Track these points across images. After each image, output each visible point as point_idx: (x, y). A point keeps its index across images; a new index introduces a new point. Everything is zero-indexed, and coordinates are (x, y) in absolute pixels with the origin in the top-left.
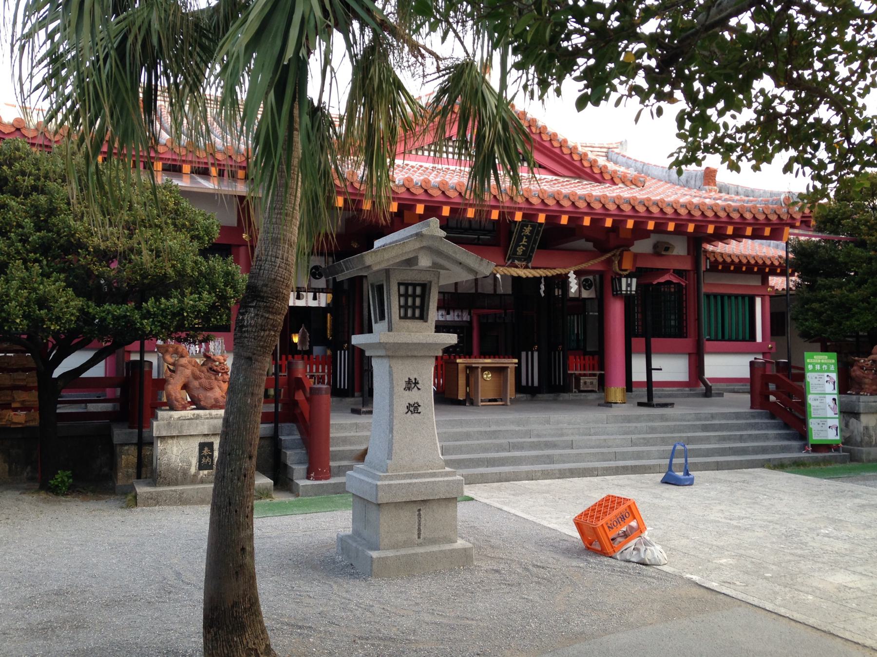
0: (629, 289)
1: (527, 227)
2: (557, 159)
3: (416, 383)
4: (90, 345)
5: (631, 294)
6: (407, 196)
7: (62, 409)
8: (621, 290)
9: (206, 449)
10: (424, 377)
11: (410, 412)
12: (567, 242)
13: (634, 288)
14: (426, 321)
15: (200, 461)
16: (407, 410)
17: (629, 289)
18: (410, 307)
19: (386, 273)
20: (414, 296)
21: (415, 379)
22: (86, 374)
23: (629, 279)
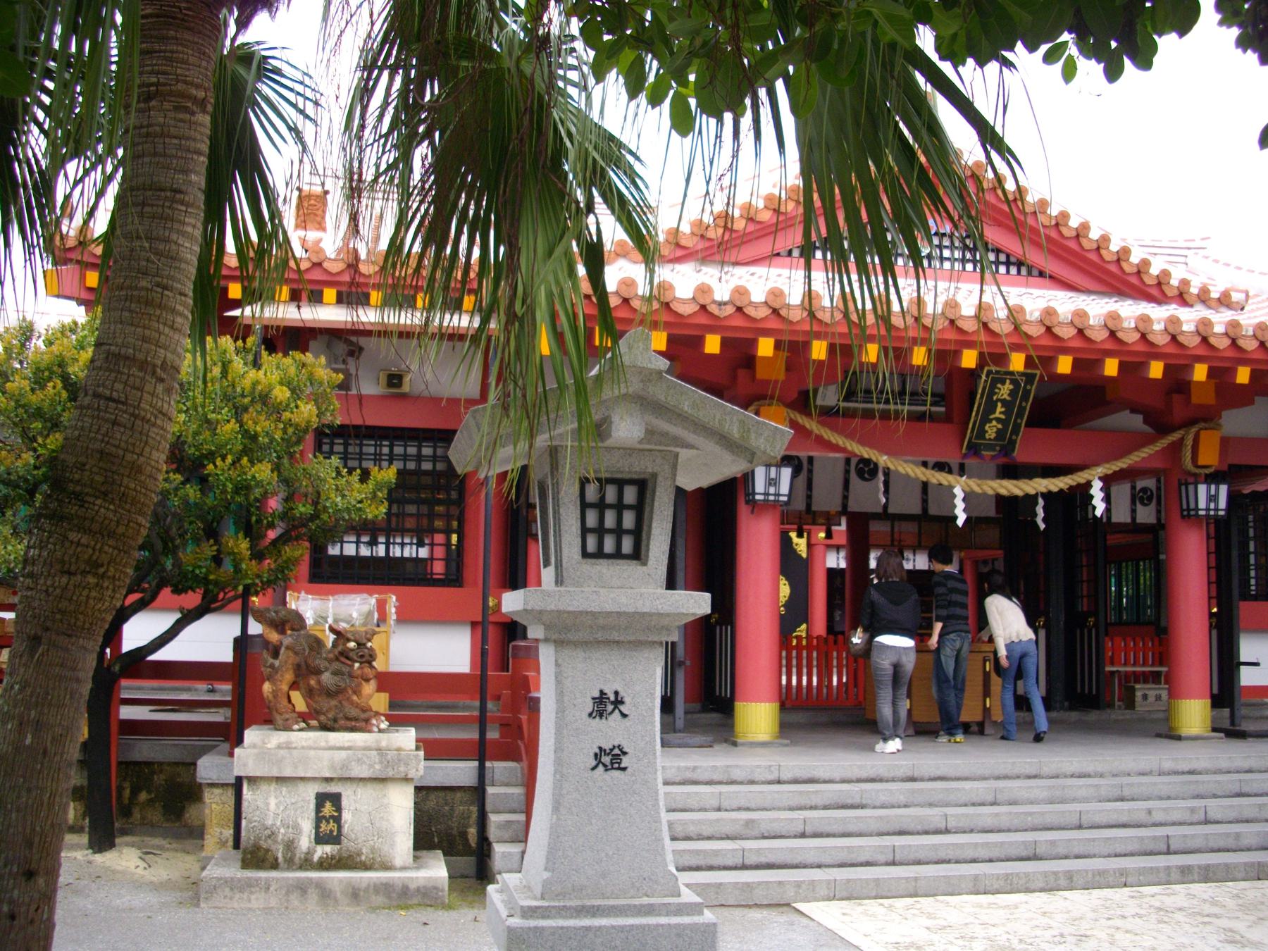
0: (1212, 506)
1: (1003, 383)
2: (1064, 255)
3: (618, 702)
4: (153, 605)
5: (1216, 515)
6: (739, 322)
7: (127, 713)
8: (1197, 509)
9: (328, 805)
10: (637, 688)
11: (601, 768)
12: (1092, 419)
13: (1222, 503)
14: (645, 564)
15: (317, 827)
16: (594, 763)
17: (1212, 506)
18: (610, 531)
19: (551, 455)
20: (620, 507)
21: (616, 693)
22: (160, 655)
23: (1213, 487)
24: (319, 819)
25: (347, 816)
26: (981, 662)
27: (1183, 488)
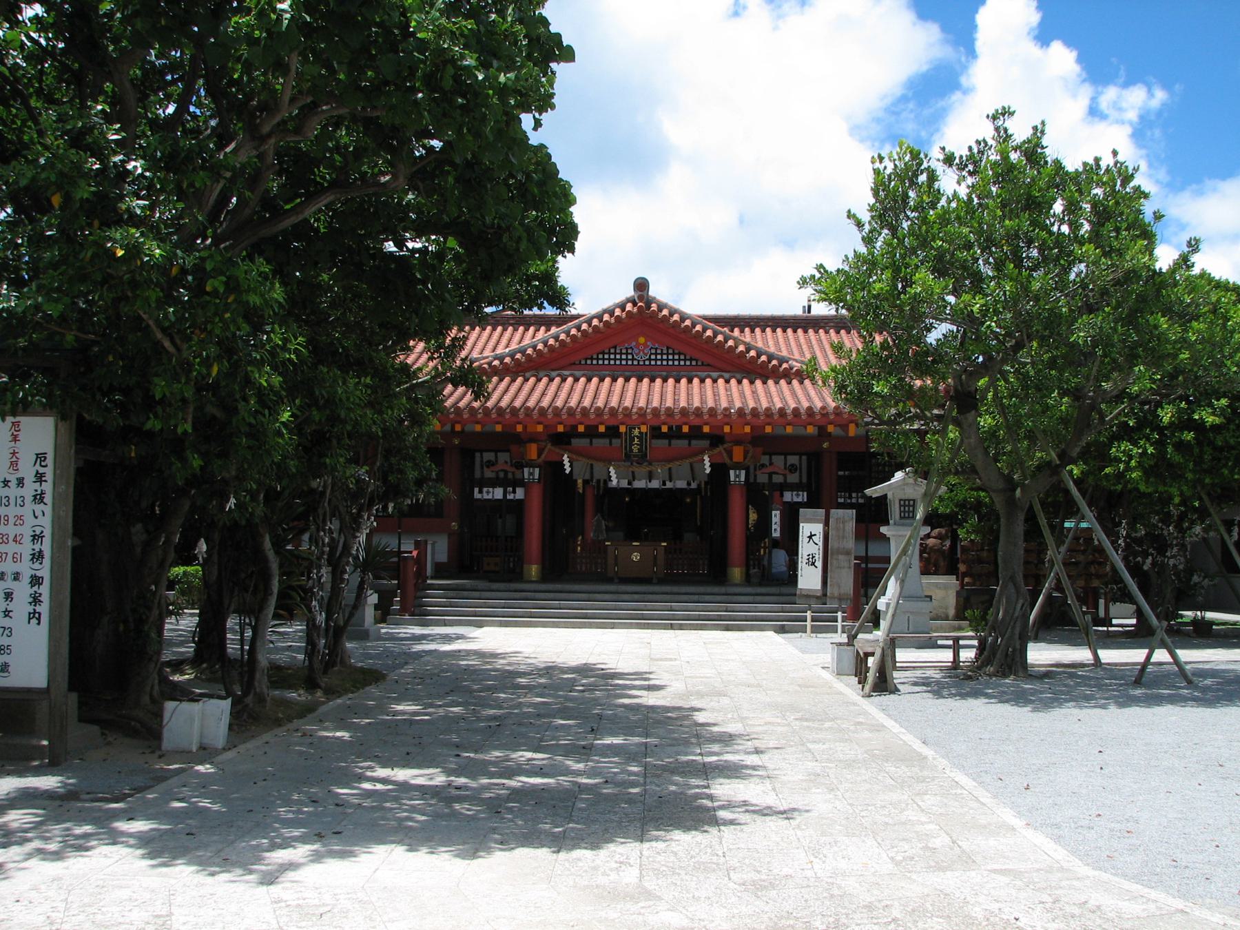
20: (909, 506)
27: (951, 642)
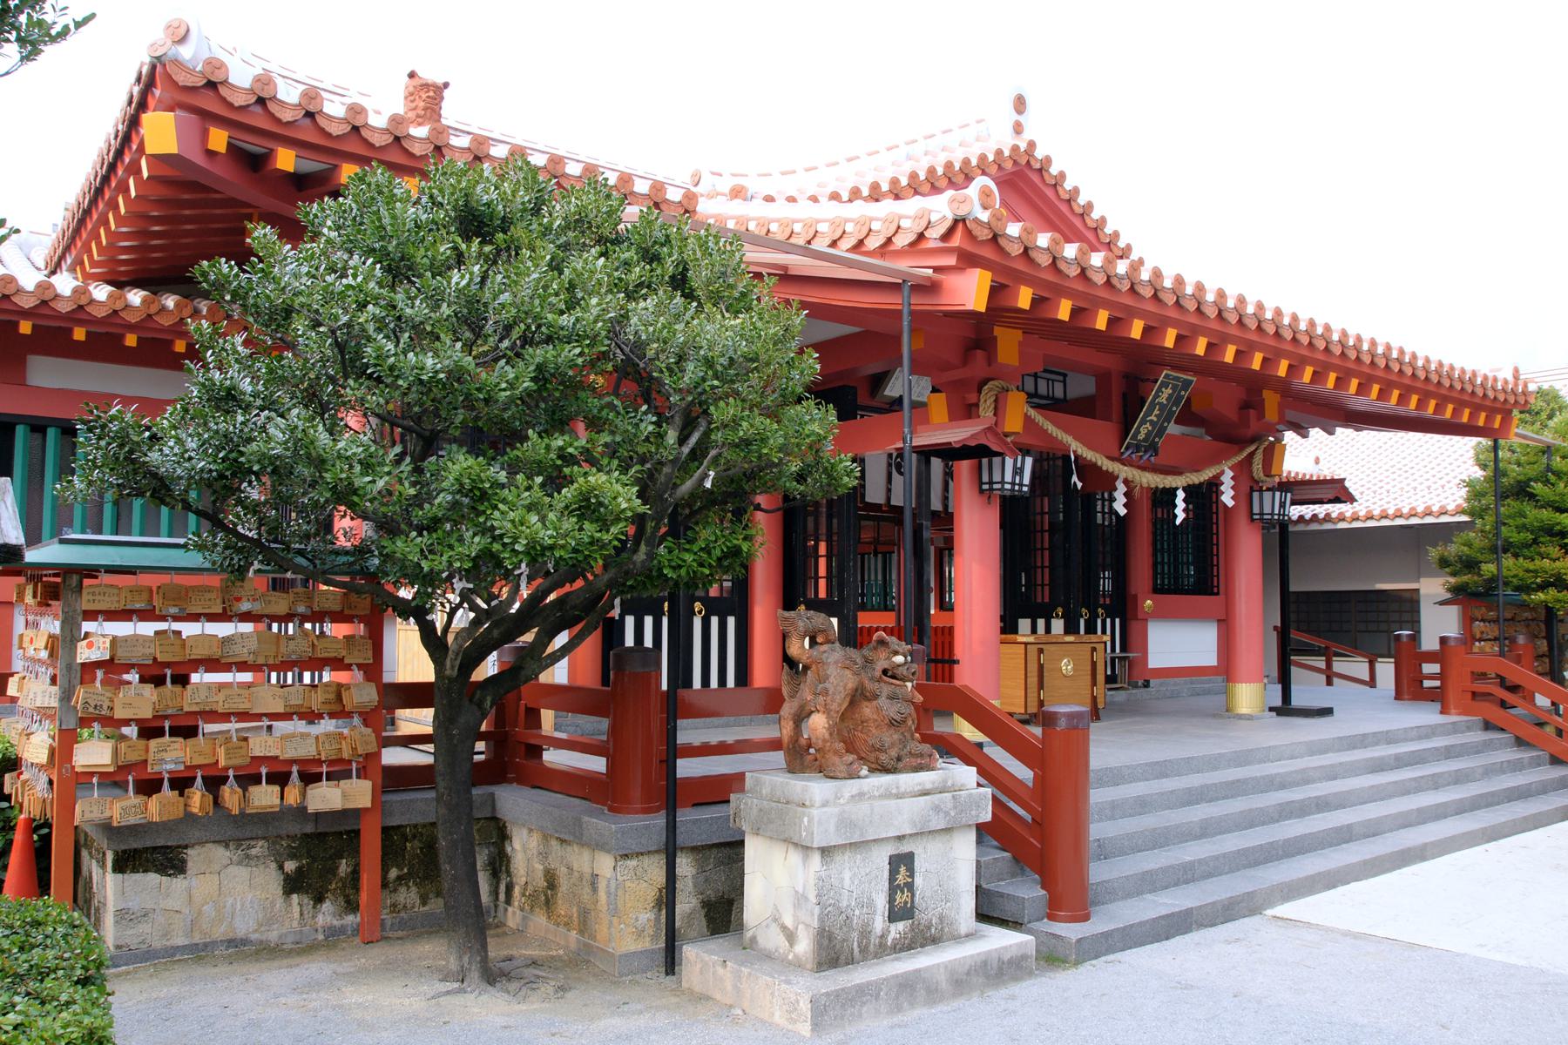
8: (1003, 482)
15: (891, 901)
24: (893, 889)
25: (919, 881)
26: (1090, 653)
27: (1256, 495)
